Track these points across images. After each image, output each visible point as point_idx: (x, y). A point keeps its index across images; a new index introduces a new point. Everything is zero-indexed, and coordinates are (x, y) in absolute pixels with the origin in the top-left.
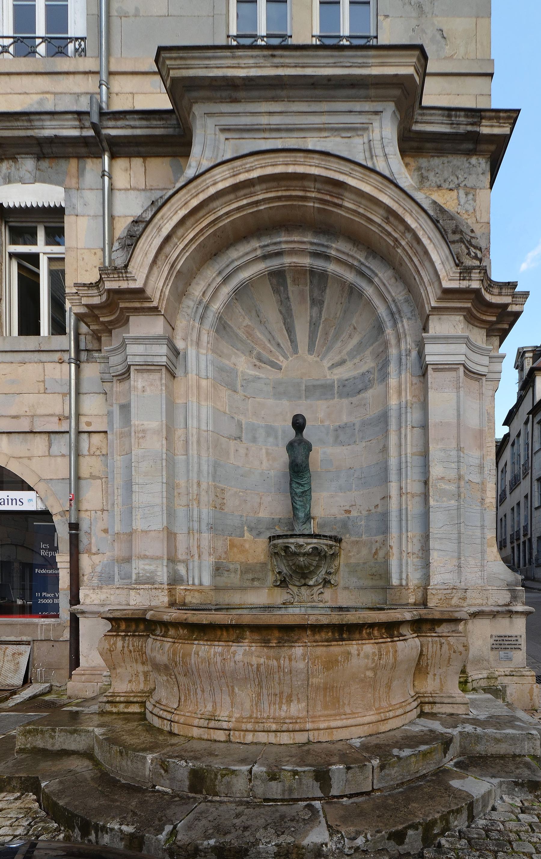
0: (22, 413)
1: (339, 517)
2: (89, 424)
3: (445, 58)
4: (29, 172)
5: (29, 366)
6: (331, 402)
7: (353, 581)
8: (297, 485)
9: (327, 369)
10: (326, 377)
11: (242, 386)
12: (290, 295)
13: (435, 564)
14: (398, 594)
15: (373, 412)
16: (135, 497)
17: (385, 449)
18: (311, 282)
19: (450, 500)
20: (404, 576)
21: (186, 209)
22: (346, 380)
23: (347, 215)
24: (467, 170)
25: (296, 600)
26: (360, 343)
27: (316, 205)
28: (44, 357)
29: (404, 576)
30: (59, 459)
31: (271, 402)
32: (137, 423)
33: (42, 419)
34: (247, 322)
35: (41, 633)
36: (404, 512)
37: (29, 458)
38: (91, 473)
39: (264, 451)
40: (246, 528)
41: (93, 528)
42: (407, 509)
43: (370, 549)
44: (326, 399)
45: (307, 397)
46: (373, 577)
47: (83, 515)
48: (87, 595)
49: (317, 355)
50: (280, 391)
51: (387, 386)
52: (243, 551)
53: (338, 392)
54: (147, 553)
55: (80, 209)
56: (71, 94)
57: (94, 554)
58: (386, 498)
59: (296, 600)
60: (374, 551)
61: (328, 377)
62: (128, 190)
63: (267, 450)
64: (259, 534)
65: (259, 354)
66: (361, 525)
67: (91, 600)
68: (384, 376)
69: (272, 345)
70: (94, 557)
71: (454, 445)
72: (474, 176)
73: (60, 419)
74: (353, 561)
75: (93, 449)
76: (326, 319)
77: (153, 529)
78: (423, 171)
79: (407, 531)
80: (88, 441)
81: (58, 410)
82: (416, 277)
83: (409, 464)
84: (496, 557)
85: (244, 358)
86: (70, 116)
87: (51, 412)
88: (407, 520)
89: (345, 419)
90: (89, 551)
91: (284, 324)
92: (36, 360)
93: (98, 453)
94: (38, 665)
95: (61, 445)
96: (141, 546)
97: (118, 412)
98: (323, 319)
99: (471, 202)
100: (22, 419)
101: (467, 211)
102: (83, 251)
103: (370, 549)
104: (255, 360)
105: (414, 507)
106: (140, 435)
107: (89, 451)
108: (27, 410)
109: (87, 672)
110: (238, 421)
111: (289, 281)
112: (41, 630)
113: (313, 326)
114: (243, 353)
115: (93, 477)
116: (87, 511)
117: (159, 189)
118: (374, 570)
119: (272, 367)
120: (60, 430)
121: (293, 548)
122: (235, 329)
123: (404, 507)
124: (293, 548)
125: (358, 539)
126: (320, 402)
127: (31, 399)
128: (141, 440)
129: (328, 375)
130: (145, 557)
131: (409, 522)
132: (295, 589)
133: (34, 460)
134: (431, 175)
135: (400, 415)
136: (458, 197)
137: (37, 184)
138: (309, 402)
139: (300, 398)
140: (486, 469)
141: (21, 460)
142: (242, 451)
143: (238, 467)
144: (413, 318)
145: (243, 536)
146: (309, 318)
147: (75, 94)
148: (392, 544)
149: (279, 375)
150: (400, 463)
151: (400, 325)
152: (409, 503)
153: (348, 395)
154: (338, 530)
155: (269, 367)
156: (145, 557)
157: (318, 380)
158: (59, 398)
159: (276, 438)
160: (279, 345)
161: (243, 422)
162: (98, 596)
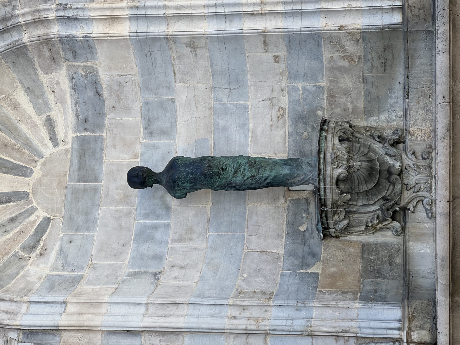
1: (288, 128)
6: (108, 142)
7: (396, 99)
8: (239, 175)
9: (57, 149)
10: (67, 150)
11: (74, 270)
14: (416, 11)
15: (133, 68)
17: (193, 42)
22: (78, 117)
25: (427, 194)
26: (29, 91)
31: (98, 234)
39: (176, 245)
40: (302, 271)
43: (342, 70)
44: (102, 150)
45: (97, 180)
46: (388, 63)
49: (33, 164)
50: (81, 218)
53: (94, 131)
58: (265, 38)
60: (345, 63)
63: (174, 241)
64: (314, 255)
65: (23, 248)
68: (87, 46)
69: (12, 230)
74: (360, 104)
85: (29, 267)
89: (135, 119)
103: (342, 70)
104: (33, 255)
110: (128, 276)
114: (23, 268)
118: (376, 63)
119: (44, 232)
121: (340, 170)
124: (340, 170)
125: (326, 95)
126: (106, 160)
129: (65, 147)
132: (407, 195)
135: (146, 18)
138: (103, 177)
139: (96, 190)
142: (176, 272)
143: (201, 277)
145: (317, 274)
148: (337, 26)
153: (100, 114)
154: (310, 129)
155: (44, 237)
157: (71, 162)
159: (155, 227)
160: (12, 220)
161: (130, 270)
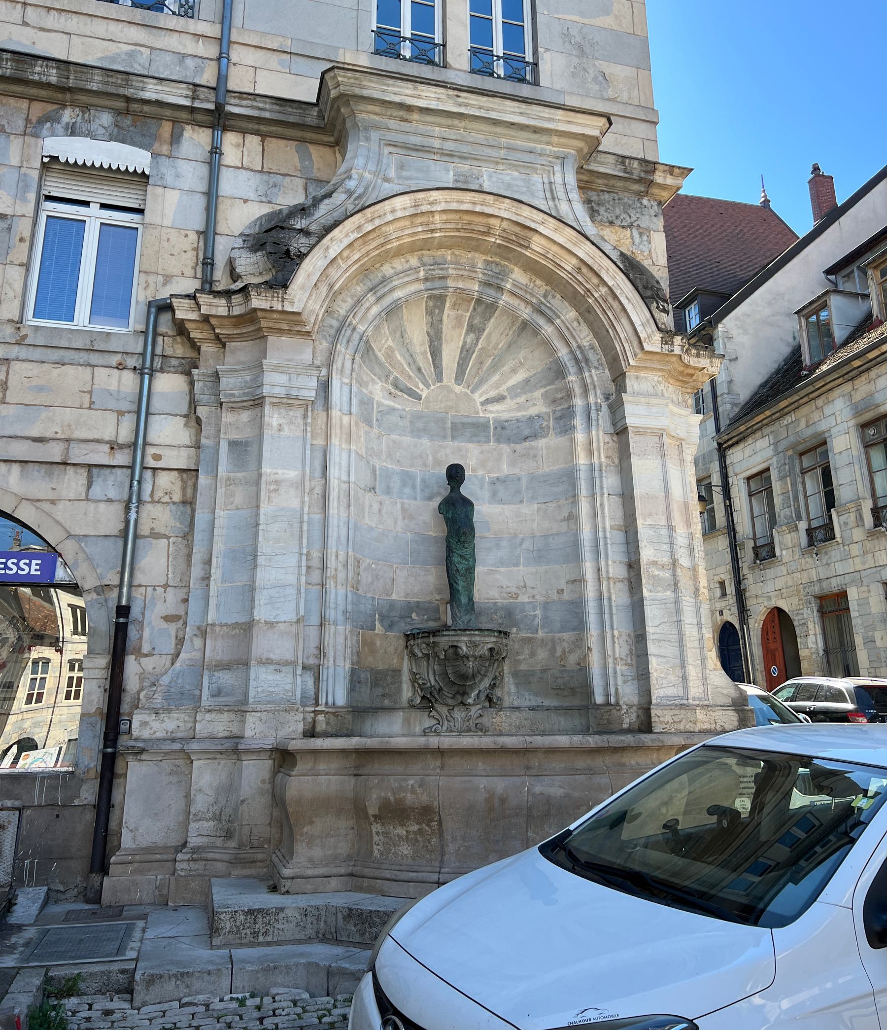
0: (49, 434)
2: (157, 457)
3: (609, 99)
4: (105, 128)
5: (70, 370)
6: (486, 447)
8: (459, 559)
9: (479, 405)
10: (478, 413)
11: (377, 420)
12: (445, 318)
13: (655, 674)
14: (606, 716)
15: (549, 467)
16: (259, 572)
18: (474, 309)
19: (665, 591)
20: (612, 691)
21: (358, 233)
22: (506, 421)
23: (532, 256)
24: (639, 210)
25: (445, 728)
26: (527, 381)
27: (498, 241)
28: (94, 358)
29: (612, 691)
30: (102, 506)
31: (407, 440)
32: (269, 471)
33: (83, 446)
34: (390, 343)
35: (41, 793)
36: (606, 602)
37: (53, 502)
38: (152, 529)
39: (399, 505)
41: (147, 614)
42: (610, 598)
44: (479, 442)
45: (453, 438)
47: (138, 594)
48: (144, 724)
50: (420, 426)
51: (572, 440)
52: (373, 651)
53: (494, 435)
54: (272, 656)
55: (169, 180)
56: (173, 52)
57: (146, 656)
59: (445, 728)
61: (481, 415)
62: (238, 168)
63: (402, 504)
64: (390, 627)
65: (396, 379)
66: (535, 616)
67: (152, 731)
69: (411, 369)
70: (144, 660)
71: (663, 522)
72: (647, 217)
73: (112, 448)
74: (523, 667)
75: (158, 494)
76: (483, 348)
77: (283, 620)
78: (593, 204)
79: (612, 628)
80: (151, 483)
81: (108, 434)
82: (610, 330)
83: (609, 541)
84: (716, 665)
86: (184, 86)
87: (97, 436)
88: (611, 614)
89: (505, 469)
90: (138, 652)
91: (430, 347)
92: (82, 361)
93: (166, 499)
94: (26, 853)
95: (111, 486)
96: (266, 644)
97: (226, 450)
98: (479, 346)
99: (645, 243)
100: (52, 444)
101: (642, 251)
102: (169, 230)
105: (619, 596)
106: (272, 487)
107: (152, 495)
108: (59, 430)
109: (137, 858)
111: (447, 305)
112: (41, 786)
113: (465, 352)
114: (379, 378)
115: (155, 535)
116: (140, 586)
117: (280, 174)
118: (560, 681)
119: (409, 396)
120: (111, 464)
122: (376, 351)
123: (605, 595)
126: (470, 446)
127: (68, 415)
128: (272, 495)
130: (268, 662)
131: (614, 617)
132: (444, 710)
133: (60, 506)
134: (602, 210)
135: (592, 478)
136: (632, 237)
137: (114, 144)
138: (456, 443)
139: (445, 437)
140: (696, 551)
141: (38, 504)
142: (376, 506)
144: (601, 367)
145: (374, 630)
146: (461, 344)
147: (179, 53)
148: (591, 646)
149: (419, 407)
150: (596, 538)
151: (587, 374)
152: (612, 591)
153: (509, 440)
154: (500, 621)
156: (268, 662)
157: (468, 416)
158: (112, 417)
159: (414, 488)
160: (419, 369)
162: (164, 725)
